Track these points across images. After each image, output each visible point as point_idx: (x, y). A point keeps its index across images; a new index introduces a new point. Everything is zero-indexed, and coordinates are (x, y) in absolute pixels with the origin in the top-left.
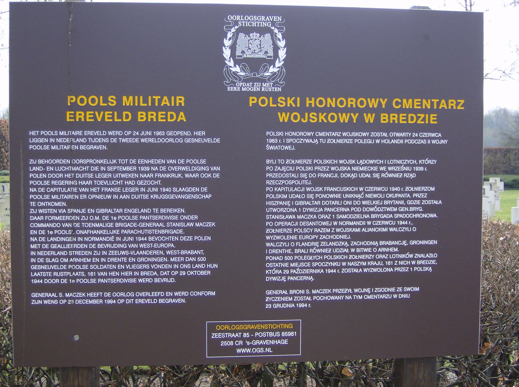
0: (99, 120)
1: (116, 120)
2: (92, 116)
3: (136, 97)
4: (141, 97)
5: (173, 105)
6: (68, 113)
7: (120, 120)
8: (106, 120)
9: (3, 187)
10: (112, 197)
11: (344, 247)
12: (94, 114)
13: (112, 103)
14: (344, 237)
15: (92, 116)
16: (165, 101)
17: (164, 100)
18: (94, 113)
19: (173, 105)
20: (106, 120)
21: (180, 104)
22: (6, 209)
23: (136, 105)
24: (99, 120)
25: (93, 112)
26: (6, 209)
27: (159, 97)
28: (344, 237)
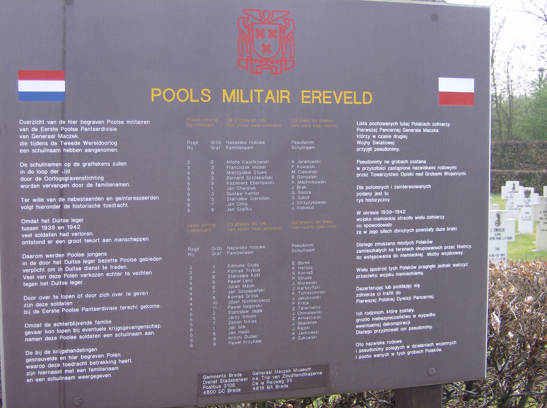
0: (338, 102)
1: (355, 103)
2: (330, 97)
3: (238, 90)
4: (242, 90)
5: (278, 102)
6: (303, 92)
7: (360, 103)
8: (345, 103)
9: (514, 185)
10: (397, 219)
11: (246, 304)
12: (332, 95)
13: (206, 98)
14: (388, 225)
15: (330, 97)
16: (270, 96)
17: (268, 95)
18: (332, 92)
19: (278, 102)
20: (345, 103)
21: (285, 100)
22: (498, 249)
23: (238, 101)
24: (338, 102)
25: (330, 92)
26: (498, 249)
27: (262, 91)
28: (388, 225)
